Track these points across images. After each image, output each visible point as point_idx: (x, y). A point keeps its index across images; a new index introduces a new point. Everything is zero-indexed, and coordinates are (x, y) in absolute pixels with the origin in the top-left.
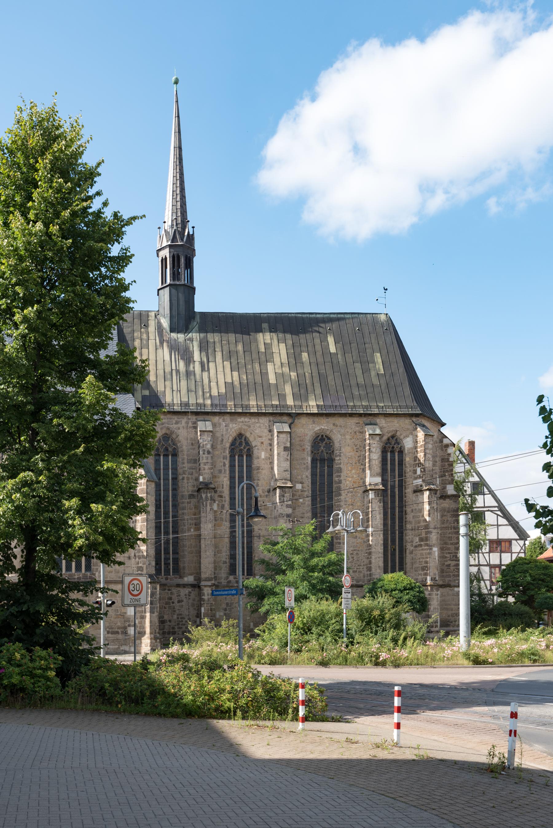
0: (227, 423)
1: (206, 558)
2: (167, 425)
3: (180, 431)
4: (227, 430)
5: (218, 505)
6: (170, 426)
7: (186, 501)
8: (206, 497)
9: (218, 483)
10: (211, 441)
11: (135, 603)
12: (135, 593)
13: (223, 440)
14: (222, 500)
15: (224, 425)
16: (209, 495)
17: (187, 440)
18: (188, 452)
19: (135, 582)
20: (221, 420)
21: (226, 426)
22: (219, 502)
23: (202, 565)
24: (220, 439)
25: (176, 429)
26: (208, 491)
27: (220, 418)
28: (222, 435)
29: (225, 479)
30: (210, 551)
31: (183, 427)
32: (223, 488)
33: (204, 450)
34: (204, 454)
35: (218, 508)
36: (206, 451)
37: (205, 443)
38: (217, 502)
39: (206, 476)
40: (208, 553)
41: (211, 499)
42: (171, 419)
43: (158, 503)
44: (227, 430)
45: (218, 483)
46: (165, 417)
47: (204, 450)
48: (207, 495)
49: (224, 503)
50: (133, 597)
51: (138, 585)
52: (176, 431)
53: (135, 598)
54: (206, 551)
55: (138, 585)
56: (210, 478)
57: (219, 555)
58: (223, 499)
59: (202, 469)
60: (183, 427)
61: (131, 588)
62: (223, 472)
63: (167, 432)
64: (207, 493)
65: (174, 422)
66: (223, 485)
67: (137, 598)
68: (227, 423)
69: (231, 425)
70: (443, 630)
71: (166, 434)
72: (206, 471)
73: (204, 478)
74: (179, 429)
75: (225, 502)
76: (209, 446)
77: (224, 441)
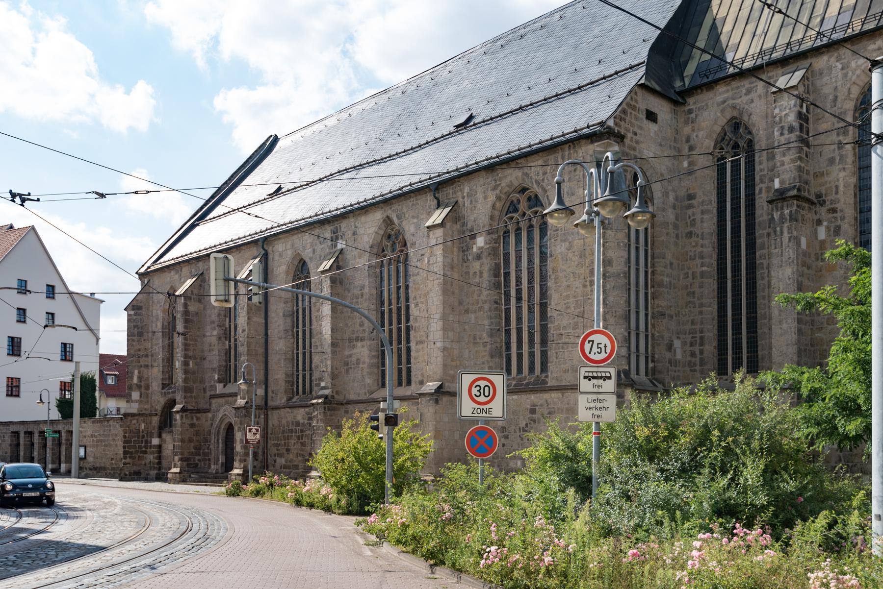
0: (845, 61)
1: (781, 335)
2: (731, 102)
3: (753, 105)
4: (845, 75)
5: (828, 228)
6: (736, 101)
7: (765, 232)
8: (782, 217)
9: (828, 185)
10: (795, 106)
11: (481, 415)
12: (482, 399)
13: (836, 97)
14: (836, 218)
15: (839, 66)
16: (786, 212)
17: (767, 117)
18: (767, 139)
19: (482, 383)
20: (833, 59)
21: (842, 69)
22: (830, 222)
23: (774, 350)
24: (831, 97)
25: (746, 104)
26: (785, 203)
27: (830, 57)
28: (836, 88)
29: (842, 174)
30: (789, 321)
31: (760, 96)
32: (837, 193)
33: (782, 128)
34: (782, 134)
35: (828, 235)
36: (786, 128)
37: (784, 113)
38: (825, 223)
39: (786, 176)
40: (785, 326)
41: (791, 219)
42: (738, 87)
43: (507, 239)
44: (845, 75)
45: (828, 185)
46: (729, 88)
47: (782, 128)
48: (782, 214)
49: (839, 223)
50: (477, 406)
51: (487, 388)
52: (746, 107)
53: (481, 407)
54: (780, 322)
55: (487, 388)
56: (794, 178)
57: (830, 327)
58: (839, 215)
59: (778, 164)
60: (760, 96)
61: (475, 391)
62: (837, 160)
63: (735, 114)
64: (782, 208)
65: (744, 91)
66: (837, 187)
67: (485, 407)
68: (845, 61)
69: (853, 64)
70: (89, 463)
71: (733, 118)
72: (787, 167)
73: (781, 183)
74: (752, 101)
75: (843, 218)
76: (792, 118)
77: (839, 99)
